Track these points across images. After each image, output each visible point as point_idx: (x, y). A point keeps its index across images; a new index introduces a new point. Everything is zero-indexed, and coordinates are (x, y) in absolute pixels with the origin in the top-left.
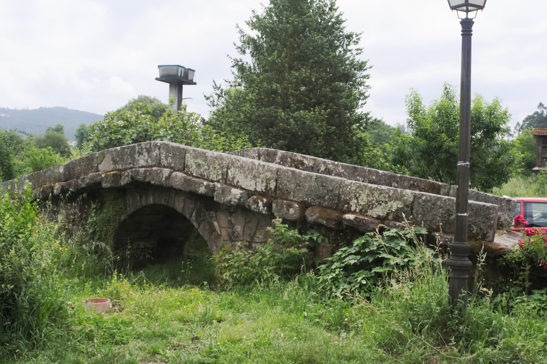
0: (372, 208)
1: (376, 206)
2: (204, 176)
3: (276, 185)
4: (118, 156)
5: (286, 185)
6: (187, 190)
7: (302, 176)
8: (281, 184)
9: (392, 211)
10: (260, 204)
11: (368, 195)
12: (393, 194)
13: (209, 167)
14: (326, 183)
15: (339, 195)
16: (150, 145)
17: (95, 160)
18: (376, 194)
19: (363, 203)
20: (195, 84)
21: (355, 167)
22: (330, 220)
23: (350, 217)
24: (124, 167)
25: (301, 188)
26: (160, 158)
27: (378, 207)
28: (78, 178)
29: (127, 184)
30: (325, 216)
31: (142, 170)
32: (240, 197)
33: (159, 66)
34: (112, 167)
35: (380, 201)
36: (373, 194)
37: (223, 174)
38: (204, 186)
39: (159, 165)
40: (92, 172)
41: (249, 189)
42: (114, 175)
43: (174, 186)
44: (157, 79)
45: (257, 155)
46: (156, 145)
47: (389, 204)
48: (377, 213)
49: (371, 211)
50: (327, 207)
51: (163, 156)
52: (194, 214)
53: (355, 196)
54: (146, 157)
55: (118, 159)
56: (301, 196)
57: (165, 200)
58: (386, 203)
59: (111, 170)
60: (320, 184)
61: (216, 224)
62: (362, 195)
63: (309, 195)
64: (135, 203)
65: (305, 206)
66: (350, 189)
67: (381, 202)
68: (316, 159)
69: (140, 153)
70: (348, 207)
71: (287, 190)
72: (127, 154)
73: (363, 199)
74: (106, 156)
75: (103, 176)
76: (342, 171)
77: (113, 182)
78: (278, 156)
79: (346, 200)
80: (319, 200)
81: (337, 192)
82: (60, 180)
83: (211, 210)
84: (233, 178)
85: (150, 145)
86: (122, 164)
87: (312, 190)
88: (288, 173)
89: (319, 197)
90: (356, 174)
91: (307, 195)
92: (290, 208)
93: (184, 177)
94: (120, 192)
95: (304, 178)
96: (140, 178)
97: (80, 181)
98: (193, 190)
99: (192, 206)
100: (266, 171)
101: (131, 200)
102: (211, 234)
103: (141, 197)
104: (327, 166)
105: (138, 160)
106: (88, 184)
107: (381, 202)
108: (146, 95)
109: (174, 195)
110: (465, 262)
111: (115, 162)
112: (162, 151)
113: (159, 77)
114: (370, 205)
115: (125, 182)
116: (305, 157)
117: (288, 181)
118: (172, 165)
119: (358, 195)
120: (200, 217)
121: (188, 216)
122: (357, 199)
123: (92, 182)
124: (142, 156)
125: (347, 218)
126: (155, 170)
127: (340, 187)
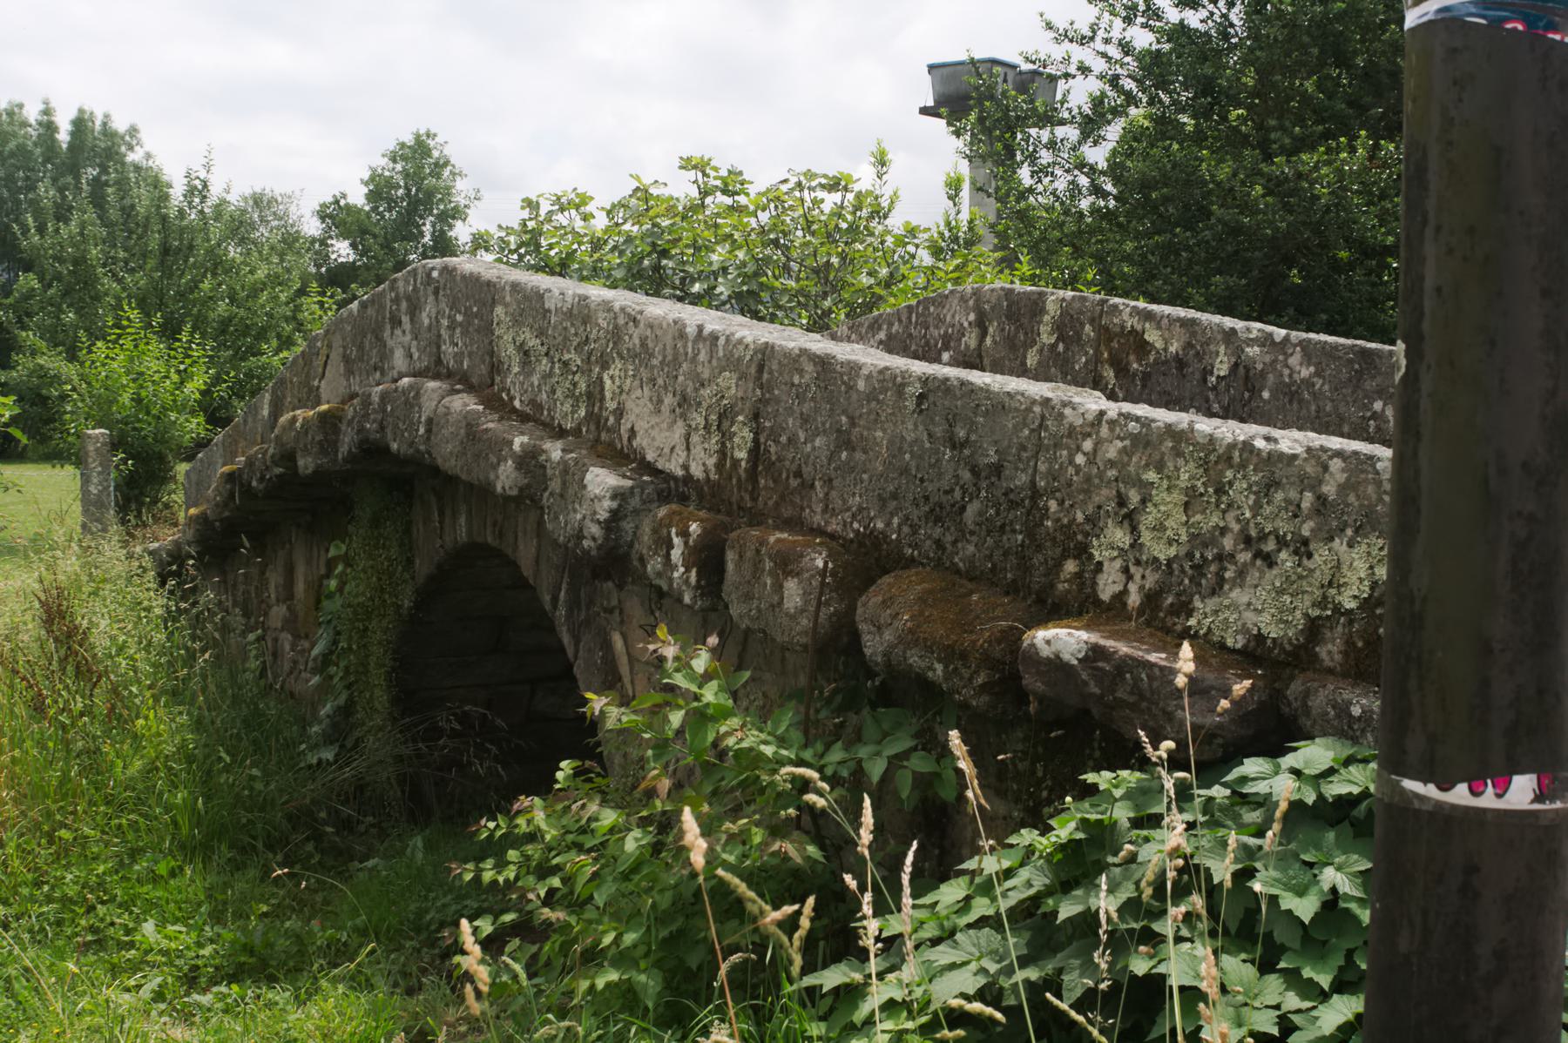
0: (1217, 589)
1: (1242, 574)
3: (756, 441)
5: (792, 440)
7: (861, 385)
8: (774, 435)
9: (1337, 609)
11: (1191, 492)
12: (1343, 488)
14: (972, 427)
18: (1240, 490)
19: (1163, 552)
21: (1364, 352)
22: (964, 656)
23: (1063, 640)
25: (859, 456)
27: (1253, 576)
32: (616, 515)
33: (932, 68)
35: (1263, 537)
36: (1220, 491)
38: (513, 455)
44: (924, 111)
45: (972, 317)
47: (1321, 556)
48: (1249, 617)
49: (1212, 603)
50: (973, 576)
53: (1122, 501)
56: (849, 508)
58: (1303, 549)
60: (939, 431)
61: (618, 641)
62: (1159, 495)
63: (894, 496)
65: (865, 561)
66: (1092, 458)
67: (1270, 546)
68: (1193, 322)
70: (1079, 575)
71: (798, 474)
73: (1167, 525)
76: (1305, 372)
78: (1046, 318)
79: (1068, 530)
81: (1022, 479)
84: (620, 413)
87: (905, 471)
88: (801, 372)
89: (936, 515)
90: (1370, 385)
91: (883, 501)
92: (789, 574)
104: (1238, 352)
107: (1270, 546)
113: (931, 103)
114: (1204, 568)
116: (1148, 316)
119: (1134, 497)
122: (1130, 520)
125: (1046, 652)
127: (1040, 446)
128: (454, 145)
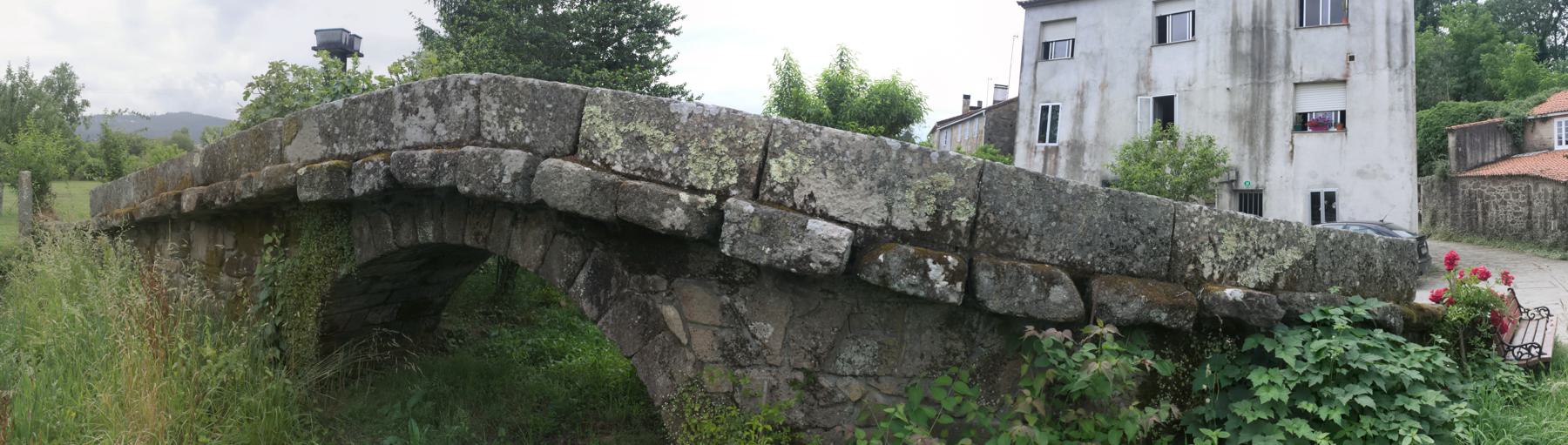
0: (1246, 267)
2: (661, 173)
4: (337, 123)
5: (1011, 214)
6: (605, 214)
8: (995, 211)
10: (936, 272)
13: (683, 149)
15: (1174, 242)
16: (444, 86)
17: (276, 136)
22: (1182, 308)
24: (357, 148)
26: (479, 121)
28: (233, 177)
29: (371, 194)
30: (1165, 300)
31: (425, 155)
34: (319, 150)
37: (742, 172)
40: (267, 164)
41: (857, 220)
42: (331, 169)
43: (550, 202)
46: (466, 85)
51: (490, 116)
52: (581, 278)
53: (1211, 241)
55: (337, 131)
56: (1062, 246)
57: (478, 234)
59: (318, 157)
61: (670, 312)
64: (372, 241)
69: (407, 111)
72: (364, 114)
74: (305, 124)
75: (302, 171)
77: (328, 187)
79: (1189, 252)
80: (1119, 258)
82: (193, 183)
83: (652, 272)
84: (791, 187)
85: (444, 86)
86: (351, 142)
91: (1081, 246)
93: (589, 174)
94: (340, 210)
95: (1074, 198)
96: (419, 176)
97: (239, 185)
99: (575, 256)
100: (936, 170)
101: (366, 231)
103: (397, 225)
105: (402, 130)
106: (260, 193)
109: (507, 222)
111: (328, 137)
112: (487, 99)
114: (1241, 263)
115: (367, 187)
117: (1020, 204)
118: (527, 140)
119: (1216, 239)
120: (608, 287)
123: (273, 186)
124: (414, 119)
126: (474, 155)
128: (852, 47)
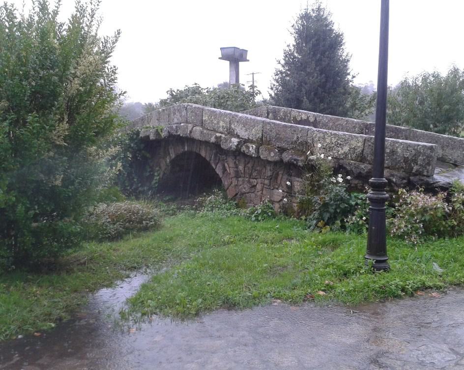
6: (204, 140)
20: (248, 61)
32: (238, 145)
39: (187, 122)
44: (220, 58)
54: (178, 117)
98: (207, 140)
102: (223, 173)
108: (400, 81)
110: (384, 196)
121: (208, 159)
